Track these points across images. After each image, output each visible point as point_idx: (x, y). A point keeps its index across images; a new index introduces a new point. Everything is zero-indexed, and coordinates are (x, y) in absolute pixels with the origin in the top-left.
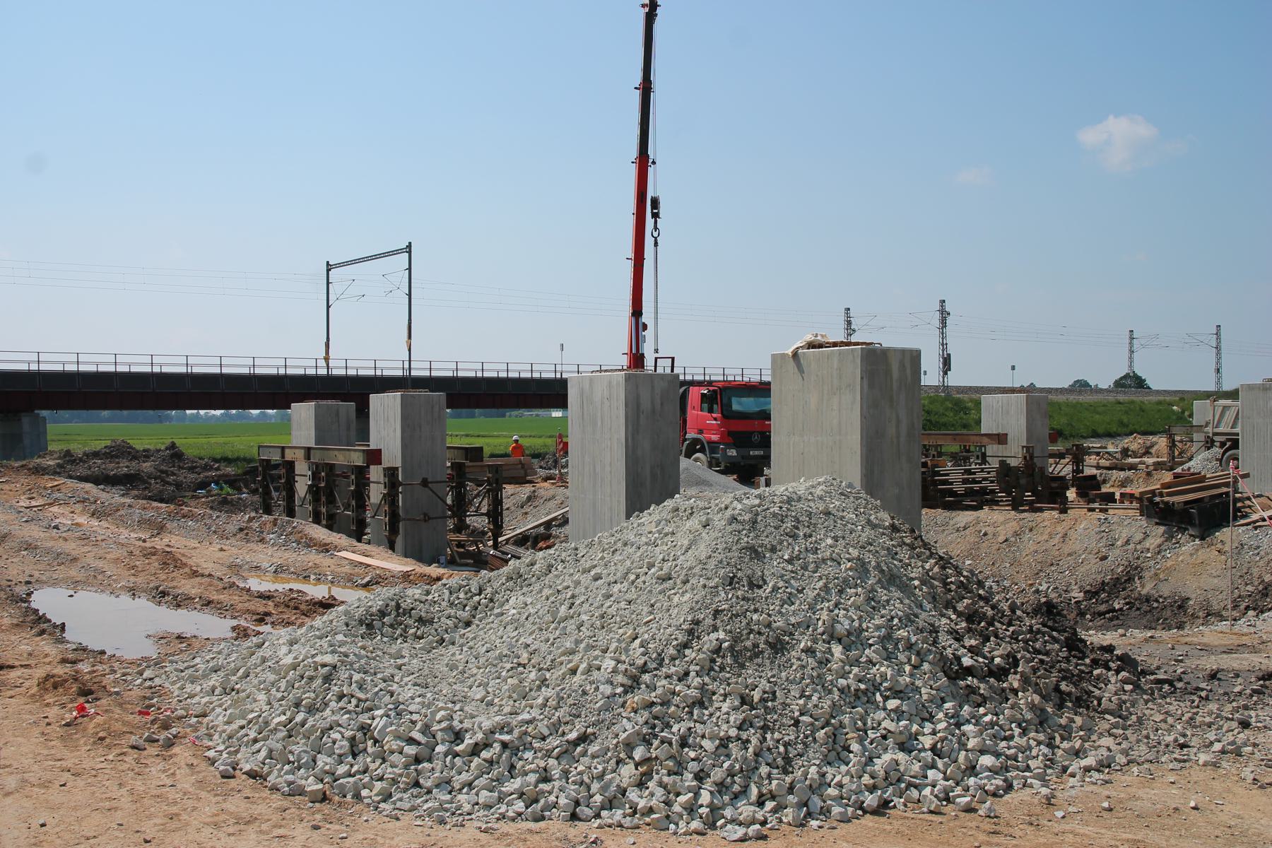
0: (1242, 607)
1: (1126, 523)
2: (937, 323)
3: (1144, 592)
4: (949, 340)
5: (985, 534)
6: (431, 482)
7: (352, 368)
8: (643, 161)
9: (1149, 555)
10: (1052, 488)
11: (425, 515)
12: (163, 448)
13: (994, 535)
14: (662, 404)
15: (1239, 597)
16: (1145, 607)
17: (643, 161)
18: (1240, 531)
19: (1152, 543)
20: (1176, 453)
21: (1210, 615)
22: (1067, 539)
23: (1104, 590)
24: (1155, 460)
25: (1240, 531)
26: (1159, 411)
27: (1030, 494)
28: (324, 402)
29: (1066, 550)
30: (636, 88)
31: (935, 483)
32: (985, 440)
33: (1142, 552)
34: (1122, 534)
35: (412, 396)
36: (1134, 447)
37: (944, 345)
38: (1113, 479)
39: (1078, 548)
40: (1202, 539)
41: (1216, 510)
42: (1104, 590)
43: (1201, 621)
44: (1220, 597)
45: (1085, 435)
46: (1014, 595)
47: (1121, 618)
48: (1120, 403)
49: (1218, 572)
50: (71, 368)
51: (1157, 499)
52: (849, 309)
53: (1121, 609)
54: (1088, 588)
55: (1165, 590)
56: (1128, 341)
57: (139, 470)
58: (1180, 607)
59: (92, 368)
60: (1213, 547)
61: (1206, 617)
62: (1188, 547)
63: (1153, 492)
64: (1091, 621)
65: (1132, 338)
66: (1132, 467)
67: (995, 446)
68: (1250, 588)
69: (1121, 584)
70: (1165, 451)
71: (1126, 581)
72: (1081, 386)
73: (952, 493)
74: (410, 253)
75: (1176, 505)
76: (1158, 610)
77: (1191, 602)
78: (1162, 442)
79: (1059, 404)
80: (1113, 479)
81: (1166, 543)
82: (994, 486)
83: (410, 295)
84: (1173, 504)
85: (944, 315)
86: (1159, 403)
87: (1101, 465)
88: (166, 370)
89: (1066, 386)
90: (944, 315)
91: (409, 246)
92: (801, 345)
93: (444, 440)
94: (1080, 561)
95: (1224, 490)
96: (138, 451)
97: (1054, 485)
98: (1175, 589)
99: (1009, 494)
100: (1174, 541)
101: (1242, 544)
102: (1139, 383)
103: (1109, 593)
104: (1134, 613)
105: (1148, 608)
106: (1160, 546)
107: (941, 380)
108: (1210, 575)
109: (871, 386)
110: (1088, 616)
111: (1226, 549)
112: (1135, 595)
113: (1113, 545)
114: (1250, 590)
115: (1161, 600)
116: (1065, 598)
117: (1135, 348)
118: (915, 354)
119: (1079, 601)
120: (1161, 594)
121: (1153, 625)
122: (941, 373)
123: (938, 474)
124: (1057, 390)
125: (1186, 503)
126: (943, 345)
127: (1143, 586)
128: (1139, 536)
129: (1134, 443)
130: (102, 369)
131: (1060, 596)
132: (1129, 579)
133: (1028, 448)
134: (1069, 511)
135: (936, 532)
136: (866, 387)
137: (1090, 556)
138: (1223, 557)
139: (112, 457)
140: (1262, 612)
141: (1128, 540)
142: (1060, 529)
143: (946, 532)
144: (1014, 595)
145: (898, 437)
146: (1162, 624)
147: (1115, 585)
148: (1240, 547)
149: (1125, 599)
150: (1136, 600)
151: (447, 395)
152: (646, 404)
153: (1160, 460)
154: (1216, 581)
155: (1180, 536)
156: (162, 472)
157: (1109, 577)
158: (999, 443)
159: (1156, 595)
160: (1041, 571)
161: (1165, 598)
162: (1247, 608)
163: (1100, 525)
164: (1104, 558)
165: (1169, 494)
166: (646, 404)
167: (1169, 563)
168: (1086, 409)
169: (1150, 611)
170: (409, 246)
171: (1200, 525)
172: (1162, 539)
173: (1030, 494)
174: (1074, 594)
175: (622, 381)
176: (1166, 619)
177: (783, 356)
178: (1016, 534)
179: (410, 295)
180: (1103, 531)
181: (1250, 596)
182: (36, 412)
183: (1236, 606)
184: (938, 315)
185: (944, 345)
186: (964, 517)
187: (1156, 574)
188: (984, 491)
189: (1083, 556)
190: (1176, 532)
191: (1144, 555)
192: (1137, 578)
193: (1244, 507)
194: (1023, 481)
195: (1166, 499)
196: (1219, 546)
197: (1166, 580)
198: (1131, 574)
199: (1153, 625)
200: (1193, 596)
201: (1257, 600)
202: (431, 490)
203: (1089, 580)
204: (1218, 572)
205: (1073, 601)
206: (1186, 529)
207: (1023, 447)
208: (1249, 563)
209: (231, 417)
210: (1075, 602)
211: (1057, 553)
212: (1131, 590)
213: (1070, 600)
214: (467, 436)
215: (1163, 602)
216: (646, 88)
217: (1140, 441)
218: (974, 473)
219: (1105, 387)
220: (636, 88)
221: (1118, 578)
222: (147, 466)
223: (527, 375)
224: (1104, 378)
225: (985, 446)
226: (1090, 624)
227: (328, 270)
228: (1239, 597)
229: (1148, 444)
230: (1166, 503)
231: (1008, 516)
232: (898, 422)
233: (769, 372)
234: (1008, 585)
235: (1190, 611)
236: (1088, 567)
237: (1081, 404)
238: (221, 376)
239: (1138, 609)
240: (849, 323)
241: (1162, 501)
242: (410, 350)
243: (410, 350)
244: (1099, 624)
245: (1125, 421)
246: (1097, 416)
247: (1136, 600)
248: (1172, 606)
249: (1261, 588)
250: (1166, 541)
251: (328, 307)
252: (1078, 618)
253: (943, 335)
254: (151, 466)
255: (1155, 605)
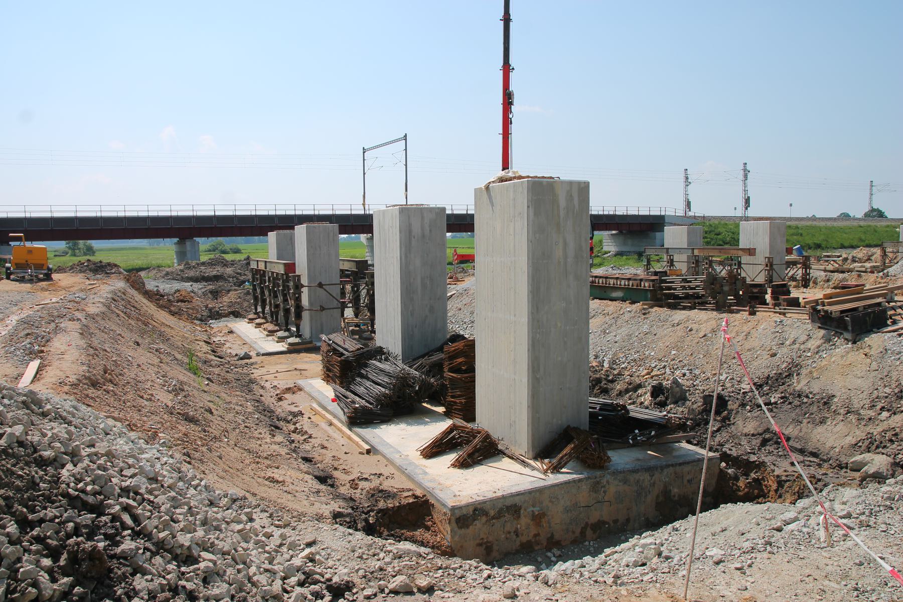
0: (878, 407)
1: (795, 326)
2: (741, 177)
3: (797, 388)
4: (749, 188)
5: (691, 330)
6: (325, 285)
7: (595, 210)
8: (507, 68)
9: (809, 354)
10: (753, 293)
11: (321, 306)
12: (243, 259)
13: (697, 331)
14: (430, 231)
15: (877, 398)
16: (796, 402)
17: (507, 68)
18: (886, 337)
19: (813, 344)
20: (887, 261)
21: (850, 412)
22: (749, 337)
23: (767, 383)
24: (872, 264)
25: (886, 337)
26: (887, 231)
27: (732, 298)
28: (281, 232)
29: (747, 346)
30: (501, 20)
31: (662, 289)
32: (740, 253)
33: (804, 352)
34: (791, 334)
35: (314, 227)
36: (860, 255)
37: (745, 191)
38: (834, 279)
39: (756, 345)
40: (854, 342)
41: (868, 319)
42: (767, 383)
43: (841, 417)
44: (861, 396)
45: (836, 247)
46: (700, 382)
47: (775, 410)
48: (861, 227)
49: (862, 374)
50: (272, 213)
51: (819, 308)
52: (687, 170)
53: (776, 403)
54: (756, 380)
55: (816, 387)
56: (869, 187)
57: (223, 273)
58: (825, 403)
59: (283, 213)
60: (861, 351)
61: (846, 414)
62: (842, 348)
63: (816, 301)
64: (750, 411)
65: (872, 186)
66: (849, 271)
67: (748, 257)
68: (887, 390)
69: (782, 379)
70: (879, 258)
71: (786, 377)
72: (845, 216)
73: (676, 297)
74: (406, 140)
75: (833, 313)
76: (807, 405)
77: (836, 400)
78: (878, 252)
79: (820, 228)
80: (834, 279)
81: (824, 345)
82: (702, 292)
83: (406, 165)
84: (831, 313)
85: (746, 173)
86: (888, 226)
87: (827, 269)
88: (34, 215)
89: (835, 216)
90: (746, 173)
91: (406, 136)
92: (493, 180)
93: (337, 255)
94: (755, 356)
95: (880, 300)
96: (227, 262)
97: (755, 290)
98: (824, 386)
99: (714, 298)
100: (831, 343)
101: (886, 350)
102: (880, 214)
103: (771, 386)
104: (786, 407)
105: (799, 403)
106: (819, 347)
107: (744, 213)
108: (856, 376)
109: (536, 214)
110: (748, 407)
111: (872, 353)
112: (790, 390)
113: (782, 344)
114: (887, 391)
115: (811, 396)
116: (736, 388)
117: (873, 192)
118: (582, 185)
119: (746, 392)
120: (812, 390)
121: (800, 418)
122: (744, 209)
123: (665, 282)
124: (826, 218)
125: (842, 312)
126: (745, 191)
127: (798, 382)
128: (803, 338)
129: (860, 253)
130: (288, 213)
131: (733, 386)
132: (789, 375)
133: (769, 258)
134: (757, 313)
135: (658, 327)
136: (531, 214)
137: (764, 352)
138: (868, 360)
139: (212, 265)
140: (895, 414)
141: (795, 341)
142: (746, 328)
143: (665, 327)
144: (700, 382)
145: (566, 257)
146: (808, 418)
147: (777, 380)
148: (884, 352)
149: (782, 393)
150: (790, 394)
151: (339, 226)
152: (416, 229)
153: (877, 264)
154: (859, 381)
155: (836, 339)
156: (238, 273)
157: (774, 372)
158: (749, 255)
159: (807, 391)
160: (725, 362)
161: (814, 395)
162: (882, 409)
163: (776, 327)
164: (773, 355)
165: (830, 304)
166: (416, 229)
167: (824, 363)
168: (839, 231)
169: (800, 406)
170: (406, 136)
171: (853, 331)
172: (822, 341)
173: (732, 298)
174: (743, 386)
175: (398, 213)
176: (812, 414)
177: (481, 188)
178: (713, 331)
179: (406, 165)
180: (778, 332)
181: (886, 397)
182: (194, 239)
183: (874, 406)
184: (742, 172)
185: (745, 191)
186: (679, 315)
187: (811, 372)
188: (696, 296)
189: (758, 353)
190: (833, 335)
191: (805, 354)
192: (795, 374)
193: (895, 315)
194: (726, 288)
195: (826, 308)
196: (867, 350)
197: (817, 378)
198: (793, 369)
199: (800, 418)
200: (838, 394)
201: (892, 402)
202: (325, 290)
203: (759, 373)
204: (862, 374)
205: (742, 391)
206: (841, 334)
207: (766, 258)
208: (890, 366)
209: (352, 238)
210: (743, 393)
211: (740, 348)
212: (789, 385)
213: (740, 390)
214: (469, 248)
215: (812, 398)
216: (507, 20)
217: (864, 252)
218: (690, 282)
219: (860, 217)
220: (501, 20)
221: (780, 374)
222: (229, 271)
223: (601, 213)
224: (858, 211)
225: (740, 257)
226: (749, 414)
227: (364, 152)
228: (877, 398)
229: (870, 253)
230: (826, 312)
231: (711, 316)
232: (565, 244)
233: (473, 207)
234: (698, 373)
235: (833, 407)
236: (760, 362)
237: (835, 227)
238: (351, 215)
239: (790, 403)
240: (687, 178)
241: (823, 309)
242: (406, 198)
243: (406, 198)
244: (756, 415)
245: (863, 238)
246: (845, 235)
247: (790, 394)
248: (818, 402)
249: (896, 391)
250: (825, 343)
251: (364, 174)
252: (740, 408)
253: (745, 185)
254: (231, 270)
255: (805, 400)
